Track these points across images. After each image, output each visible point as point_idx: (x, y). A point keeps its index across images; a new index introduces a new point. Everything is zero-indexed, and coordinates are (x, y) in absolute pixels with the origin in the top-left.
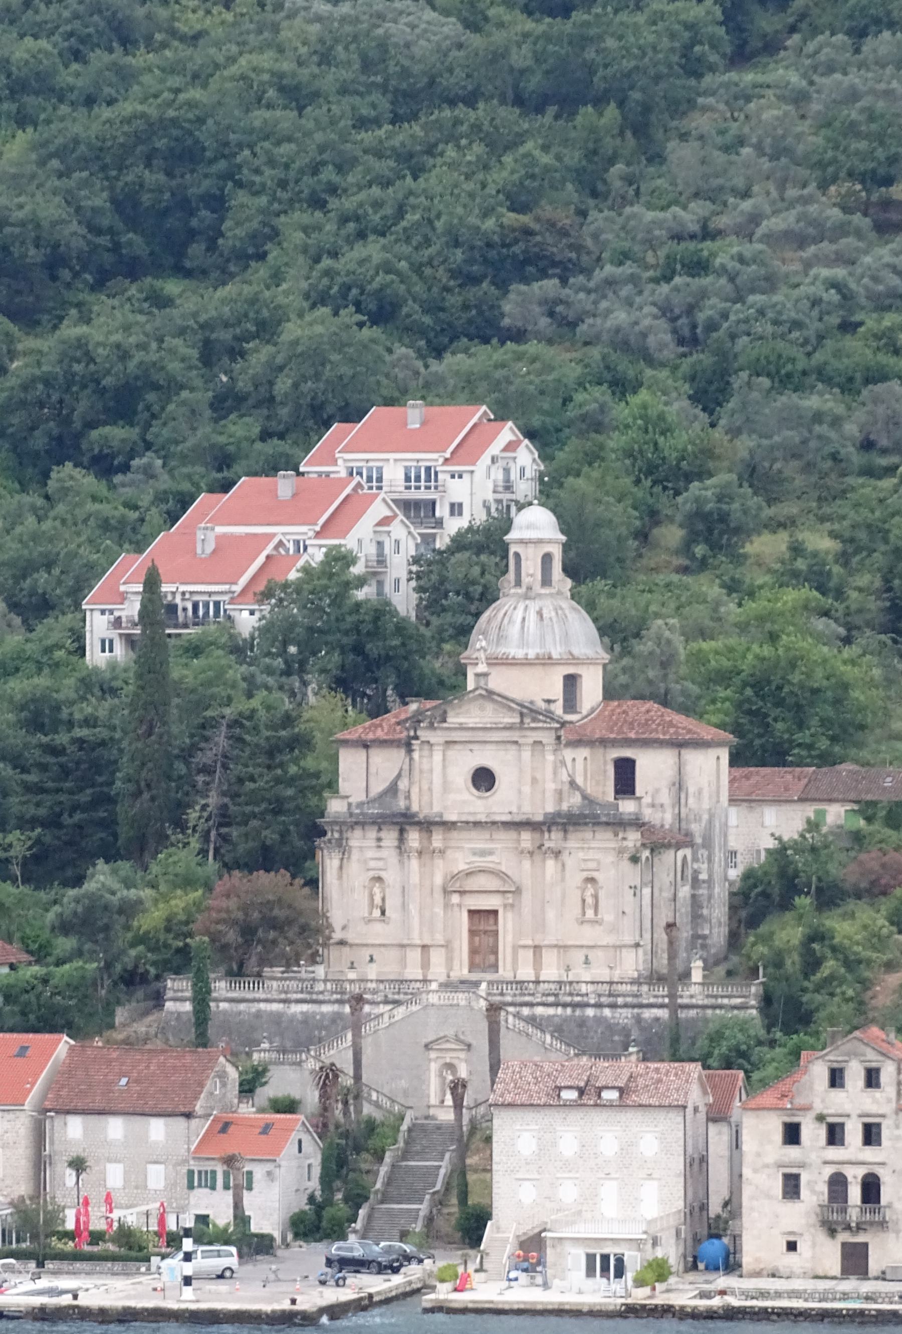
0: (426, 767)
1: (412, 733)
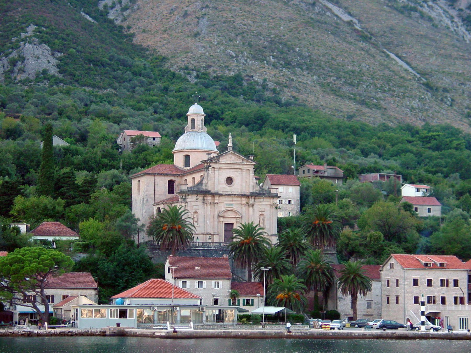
0: (212, 176)
1: (209, 165)
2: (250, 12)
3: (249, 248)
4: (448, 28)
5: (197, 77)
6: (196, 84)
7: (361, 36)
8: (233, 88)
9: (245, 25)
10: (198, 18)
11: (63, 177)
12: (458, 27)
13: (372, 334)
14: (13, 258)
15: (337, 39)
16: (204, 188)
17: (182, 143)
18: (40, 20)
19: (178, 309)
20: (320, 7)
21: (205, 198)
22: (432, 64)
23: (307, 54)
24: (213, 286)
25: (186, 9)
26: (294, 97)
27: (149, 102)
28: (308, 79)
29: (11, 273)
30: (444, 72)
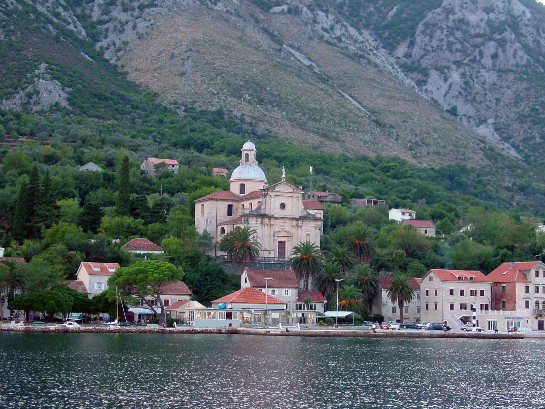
2: (227, 55)
3: (308, 262)
4: (391, 73)
5: (185, 111)
6: (185, 117)
7: (321, 79)
8: (217, 121)
9: (223, 67)
10: (184, 60)
11: (137, 201)
12: (398, 73)
13: (438, 334)
14: (138, 269)
15: (301, 81)
16: (262, 212)
17: (237, 174)
18: (49, 59)
19: (270, 312)
20: (286, 53)
21: (263, 220)
22: (379, 104)
23: (276, 93)
24: (283, 294)
25: (173, 51)
26: (267, 130)
27: (149, 132)
28: (277, 114)
29: (137, 281)
30: (389, 111)
